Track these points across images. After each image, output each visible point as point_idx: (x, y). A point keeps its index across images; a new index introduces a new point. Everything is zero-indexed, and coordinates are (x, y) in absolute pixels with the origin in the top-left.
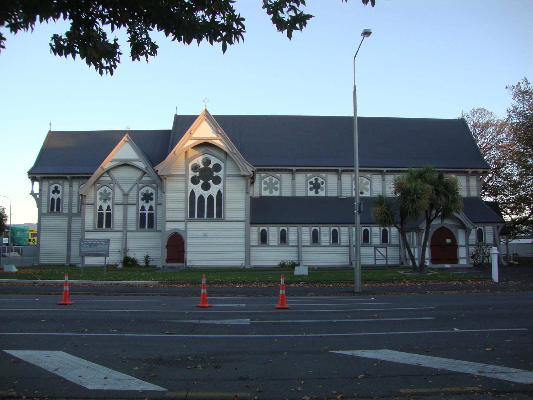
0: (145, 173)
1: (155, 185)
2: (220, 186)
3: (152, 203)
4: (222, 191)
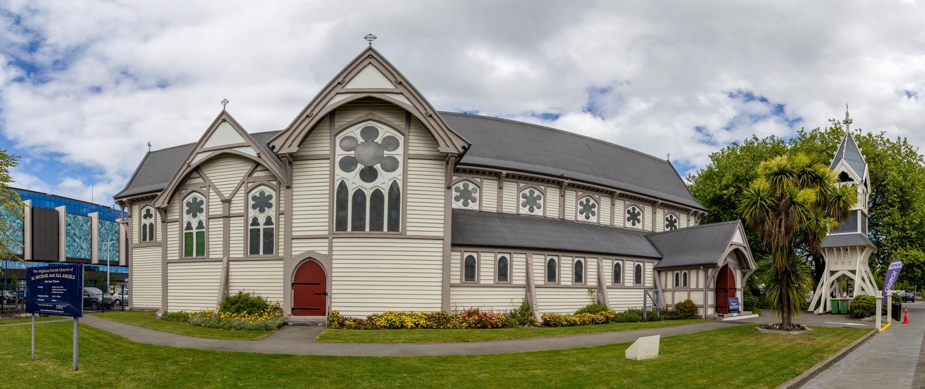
0: (258, 164)
1: (274, 183)
2: (398, 174)
3: (271, 212)
4: (400, 184)
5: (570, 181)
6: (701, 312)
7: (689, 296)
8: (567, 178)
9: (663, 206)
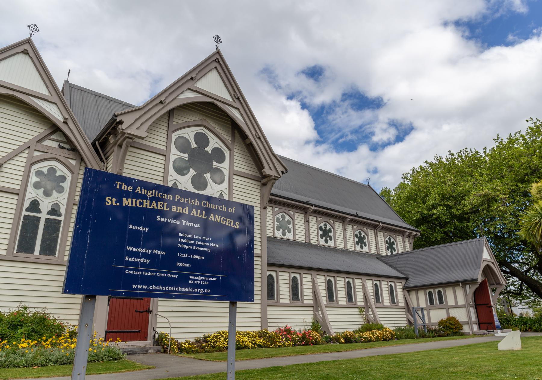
5: (314, 208)
6: (466, 329)
7: (448, 313)
8: (312, 205)
9: (384, 229)
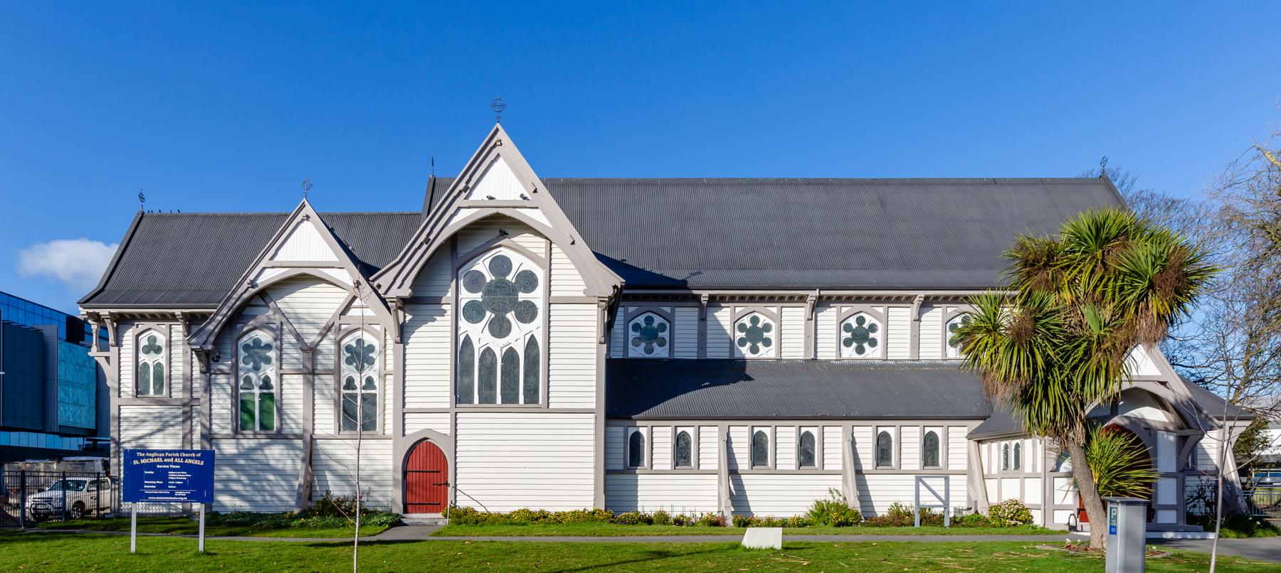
2: (536, 327)
